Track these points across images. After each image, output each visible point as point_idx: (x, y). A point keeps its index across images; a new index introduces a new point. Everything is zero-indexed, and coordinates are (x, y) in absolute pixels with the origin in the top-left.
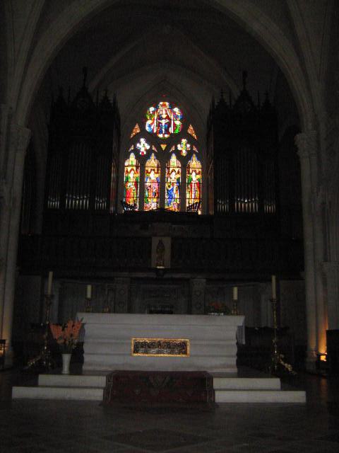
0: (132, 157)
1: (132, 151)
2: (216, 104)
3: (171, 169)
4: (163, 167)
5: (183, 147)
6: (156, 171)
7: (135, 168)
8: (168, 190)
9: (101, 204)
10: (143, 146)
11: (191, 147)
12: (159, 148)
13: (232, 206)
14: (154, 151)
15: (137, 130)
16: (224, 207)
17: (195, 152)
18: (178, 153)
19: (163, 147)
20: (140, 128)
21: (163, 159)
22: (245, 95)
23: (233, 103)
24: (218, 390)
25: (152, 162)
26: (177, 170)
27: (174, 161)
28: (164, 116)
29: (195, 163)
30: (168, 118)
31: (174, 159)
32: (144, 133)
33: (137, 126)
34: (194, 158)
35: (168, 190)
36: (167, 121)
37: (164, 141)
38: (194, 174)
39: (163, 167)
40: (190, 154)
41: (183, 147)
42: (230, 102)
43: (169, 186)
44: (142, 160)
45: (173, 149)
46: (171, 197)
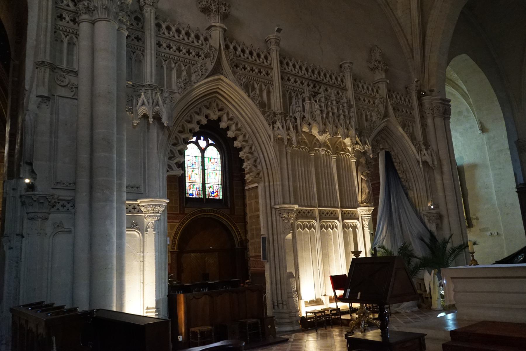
11: (192, 142)
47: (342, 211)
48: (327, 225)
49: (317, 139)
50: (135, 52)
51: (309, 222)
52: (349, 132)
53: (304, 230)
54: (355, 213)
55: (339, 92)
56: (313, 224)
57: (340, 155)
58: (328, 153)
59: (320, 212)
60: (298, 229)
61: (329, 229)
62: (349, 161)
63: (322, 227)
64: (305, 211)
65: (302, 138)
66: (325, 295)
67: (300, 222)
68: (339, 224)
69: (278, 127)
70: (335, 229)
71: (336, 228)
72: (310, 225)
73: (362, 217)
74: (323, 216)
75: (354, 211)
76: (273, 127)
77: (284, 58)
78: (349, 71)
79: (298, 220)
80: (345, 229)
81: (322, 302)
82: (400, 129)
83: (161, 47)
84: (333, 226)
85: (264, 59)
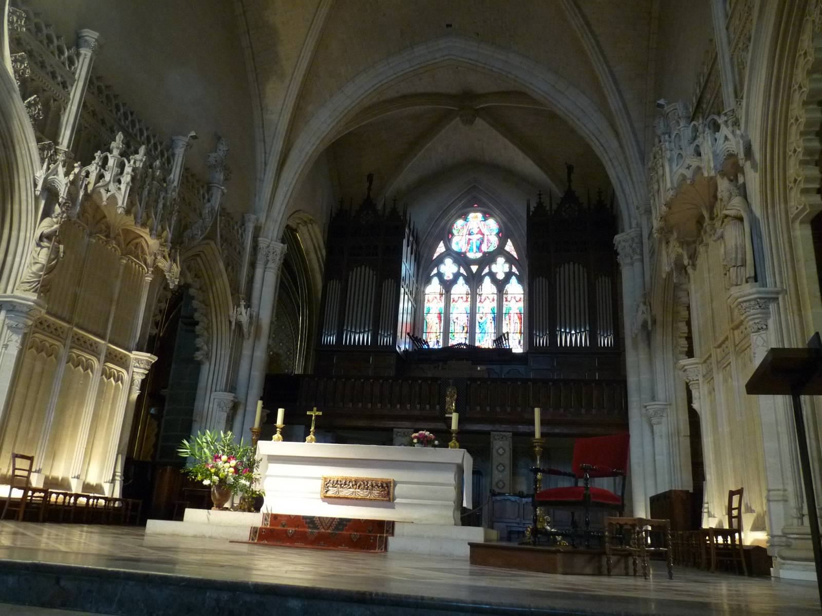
0: (435, 281)
1: (435, 275)
2: (532, 209)
3: (483, 297)
4: (474, 295)
5: (500, 267)
6: (465, 299)
7: (438, 296)
8: (479, 323)
9: (386, 340)
10: (449, 268)
11: (511, 268)
12: (468, 270)
13: (339, 338)
14: (462, 275)
15: (441, 248)
16: (542, 341)
17: (514, 274)
18: (492, 275)
19: (474, 268)
20: (446, 246)
21: (474, 281)
22: (570, 195)
23: (555, 207)
24: (112, 495)
25: (461, 288)
26: (491, 297)
27: (488, 287)
28: (475, 231)
29: (515, 289)
30: (480, 232)
31: (487, 280)
32: (449, 252)
33: (442, 244)
34: (514, 280)
35: (479, 323)
36: (480, 236)
37: (474, 262)
38: (513, 301)
39: (474, 295)
40: (508, 275)
41: (500, 267)
42: (551, 205)
43: (481, 318)
44: (447, 286)
45: (486, 270)
46: (483, 332)
51: (118, 371)
52: (163, 232)
54: (124, 360)
57: (132, 262)
58: (115, 251)
61: (112, 379)
62: (142, 277)
63: (104, 372)
66: (78, 477)
67: (75, 353)
70: (120, 382)
71: (122, 383)
73: (133, 372)
75: (125, 355)
76: (48, 168)
77: (47, 26)
80: (104, 376)
82: (222, 265)
84: (119, 376)
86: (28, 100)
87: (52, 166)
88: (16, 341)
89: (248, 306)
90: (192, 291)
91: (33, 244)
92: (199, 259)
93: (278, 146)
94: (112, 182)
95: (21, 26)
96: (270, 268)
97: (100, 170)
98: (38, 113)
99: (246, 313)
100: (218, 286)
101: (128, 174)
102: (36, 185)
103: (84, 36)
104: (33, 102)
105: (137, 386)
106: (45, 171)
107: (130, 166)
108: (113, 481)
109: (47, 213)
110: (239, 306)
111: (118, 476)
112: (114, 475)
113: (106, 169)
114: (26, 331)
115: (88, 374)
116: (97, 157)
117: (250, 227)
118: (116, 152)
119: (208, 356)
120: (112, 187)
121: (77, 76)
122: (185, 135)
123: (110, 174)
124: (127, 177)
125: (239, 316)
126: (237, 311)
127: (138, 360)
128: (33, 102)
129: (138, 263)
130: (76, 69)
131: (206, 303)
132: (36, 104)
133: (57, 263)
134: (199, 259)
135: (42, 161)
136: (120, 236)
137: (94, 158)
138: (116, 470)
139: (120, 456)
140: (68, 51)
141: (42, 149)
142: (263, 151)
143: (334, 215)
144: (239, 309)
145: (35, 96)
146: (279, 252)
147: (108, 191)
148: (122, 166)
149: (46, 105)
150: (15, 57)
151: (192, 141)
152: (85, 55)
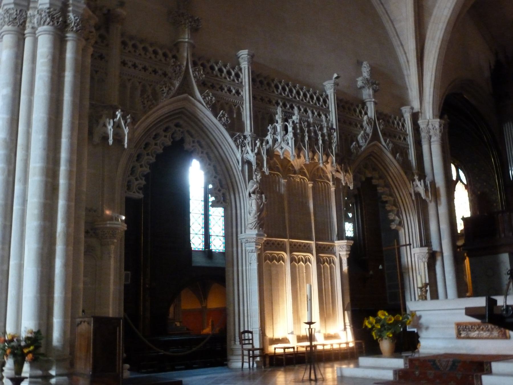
47: (317, 245)
48: (306, 258)
49: (292, 165)
50: (152, 85)
51: (304, 256)
53: (279, 263)
54: (331, 248)
55: (321, 113)
56: (282, 256)
59: (291, 244)
60: (265, 260)
64: (301, 244)
65: (275, 162)
68: (313, 258)
69: (247, 151)
70: (308, 263)
72: (299, 259)
74: (295, 248)
76: (242, 151)
78: (373, 100)
79: (265, 251)
81: (289, 341)
83: (147, 71)
85: (218, 72)
86: (219, 116)
87: (244, 149)
88: (255, 260)
89: (422, 176)
90: (374, 182)
91: (248, 199)
92: (371, 157)
93: (411, 45)
94: (282, 142)
95: (202, 75)
96: (434, 141)
97: (273, 137)
98: (227, 120)
99: (421, 184)
100: (392, 171)
101: (290, 132)
102: (238, 162)
103: (241, 56)
104: (222, 115)
105: (345, 264)
106: (240, 154)
107: (290, 127)
108: (345, 329)
109: (250, 178)
110: (413, 180)
111: (348, 325)
112: (345, 325)
113: (277, 134)
114: (259, 253)
115: (308, 265)
116: (270, 129)
117: (407, 117)
118: (280, 121)
119: (401, 224)
120: (284, 145)
121: (244, 84)
122: (331, 79)
123: (280, 137)
124: (290, 135)
125: (416, 189)
126: (413, 185)
127: (341, 246)
128: (222, 115)
129: (322, 182)
130: (242, 79)
131: (387, 185)
132: (224, 115)
133: (263, 205)
134: (371, 157)
135: (238, 147)
136: (304, 169)
137: (268, 131)
138: (346, 322)
139: (346, 312)
140: (234, 71)
141: (235, 141)
142: (403, 52)
143: (493, 67)
144: (414, 183)
145: (222, 111)
146: (437, 126)
147: (282, 148)
148: (286, 129)
149: (230, 113)
150: (204, 95)
151: (337, 80)
152: (245, 67)
